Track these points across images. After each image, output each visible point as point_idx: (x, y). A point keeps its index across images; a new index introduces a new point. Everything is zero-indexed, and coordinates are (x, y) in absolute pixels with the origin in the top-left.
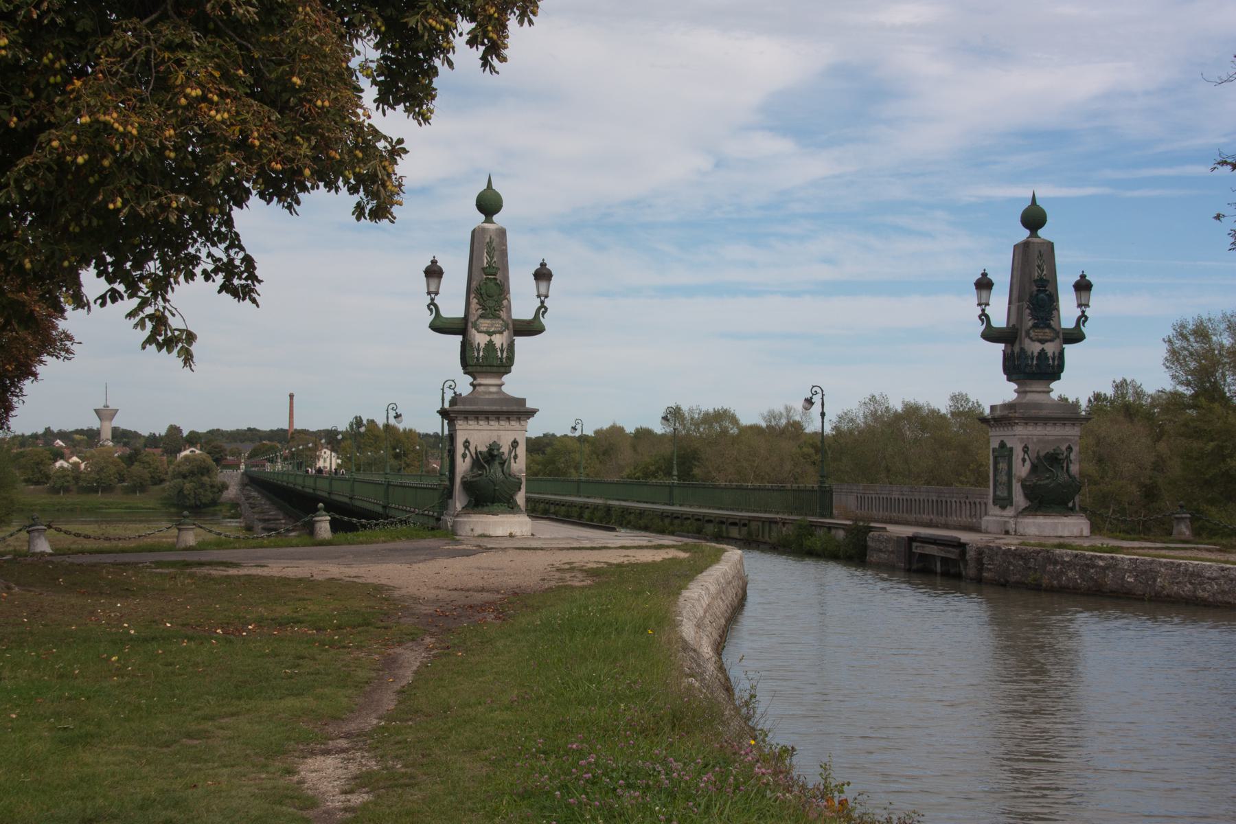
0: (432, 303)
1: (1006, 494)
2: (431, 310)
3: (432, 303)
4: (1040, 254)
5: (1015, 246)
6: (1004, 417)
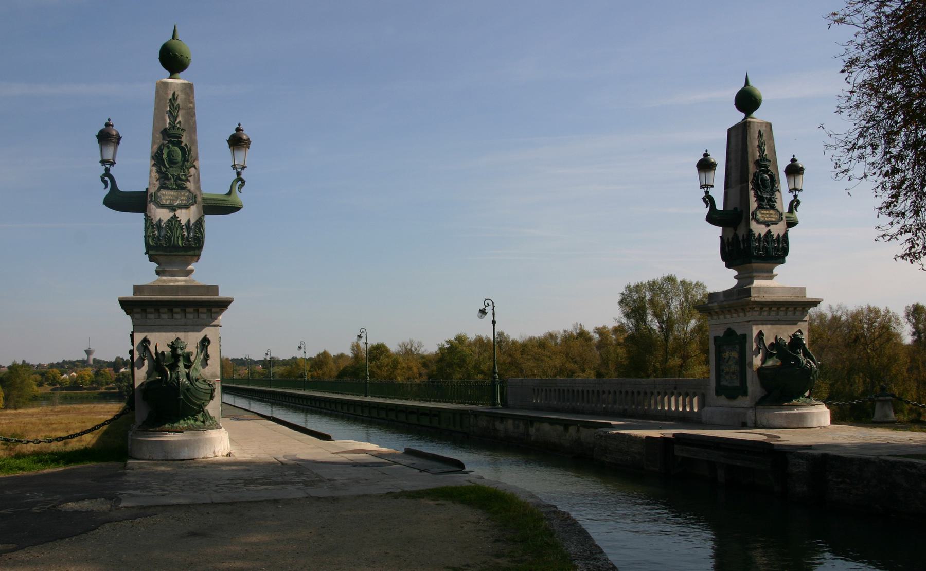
0: (107, 173)
1: (737, 383)
2: (105, 182)
3: (107, 173)
4: (760, 135)
5: (729, 130)
6: (713, 305)
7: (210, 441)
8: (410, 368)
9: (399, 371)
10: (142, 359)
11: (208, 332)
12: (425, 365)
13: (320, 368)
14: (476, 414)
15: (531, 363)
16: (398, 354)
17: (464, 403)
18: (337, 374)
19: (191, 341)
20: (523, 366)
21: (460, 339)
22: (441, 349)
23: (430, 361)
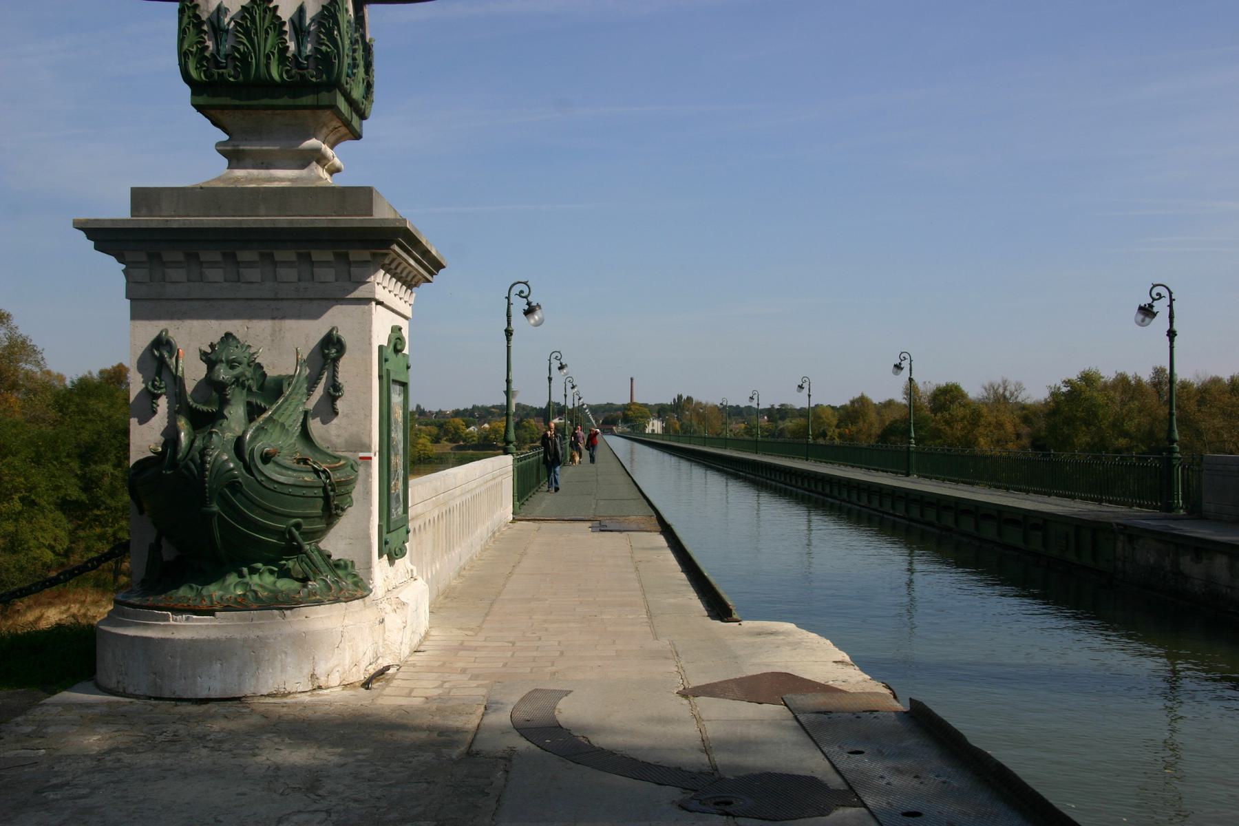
7: (304, 644)
8: (1000, 425)
9: (981, 430)
10: (150, 396)
11: (338, 318)
12: (1026, 420)
13: (854, 422)
14: (1131, 534)
15: (1218, 422)
16: (983, 402)
17: (1100, 502)
18: (879, 432)
19: (280, 344)
20: (1203, 425)
21: (1088, 378)
22: (1055, 394)
23: (1035, 413)
